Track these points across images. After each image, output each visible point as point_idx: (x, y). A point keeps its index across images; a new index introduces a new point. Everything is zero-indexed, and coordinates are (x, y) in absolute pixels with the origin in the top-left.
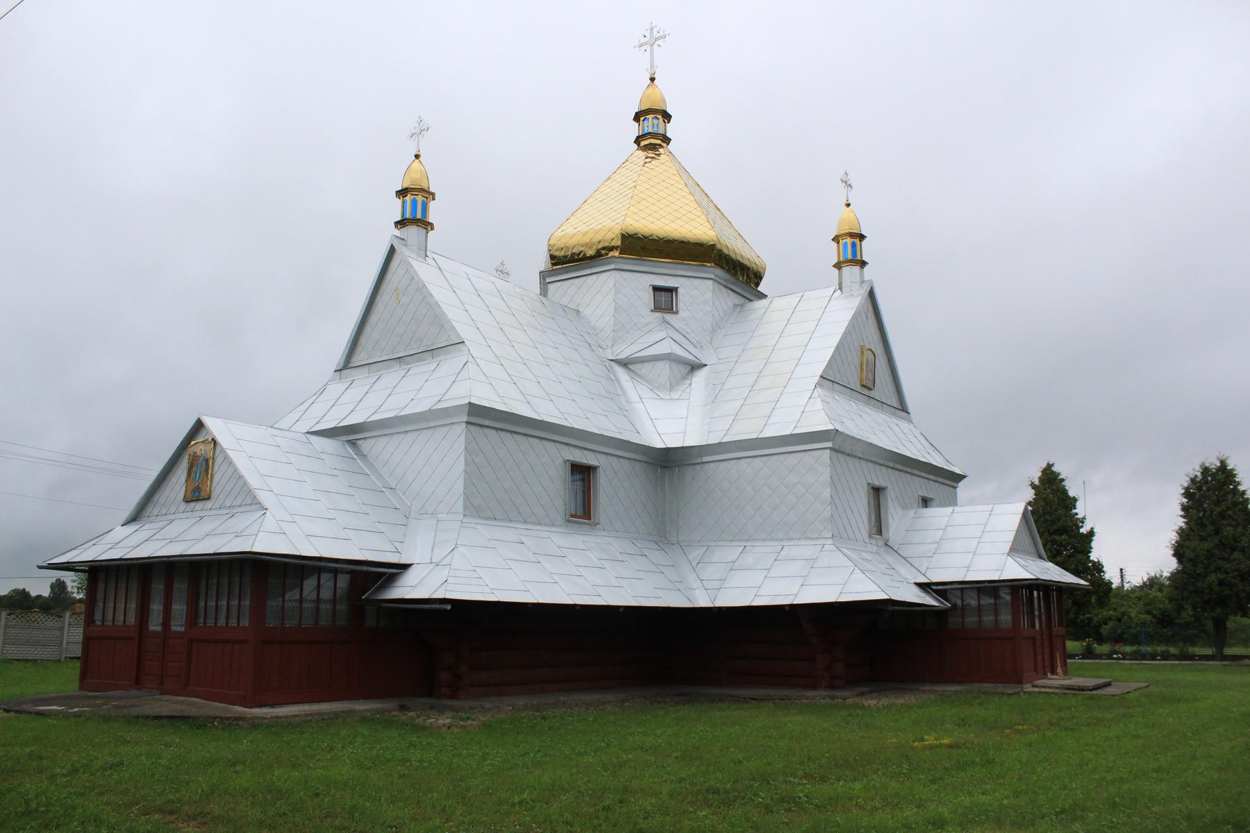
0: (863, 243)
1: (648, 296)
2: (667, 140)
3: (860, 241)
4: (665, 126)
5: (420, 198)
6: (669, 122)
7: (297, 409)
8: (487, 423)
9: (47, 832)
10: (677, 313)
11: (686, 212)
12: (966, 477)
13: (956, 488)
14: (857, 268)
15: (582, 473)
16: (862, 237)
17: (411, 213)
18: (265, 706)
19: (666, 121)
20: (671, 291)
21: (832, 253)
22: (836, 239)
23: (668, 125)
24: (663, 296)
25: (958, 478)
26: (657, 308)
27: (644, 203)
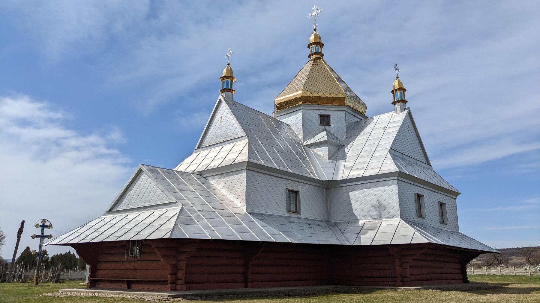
0: (405, 93)
1: (318, 118)
2: (323, 55)
3: (404, 92)
4: (321, 49)
5: (230, 80)
6: (323, 48)
7: (202, 167)
8: (265, 172)
9: (221, 302)
10: (330, 125)
11: (323, 81)
12: (460, 194)
13: (456, 199)
14: (402, 104)
15: (293, 195)
16: (405, 90)
17: (400, 98)
18: (442, 192)
19: (322, 47)
20: (328, 116)
21: (390, 98)
22: (393, 92)
23: (322, 49)
24: (324, 119)
25: (457, 194)
26: (321, 123)
27: (317, 78)
